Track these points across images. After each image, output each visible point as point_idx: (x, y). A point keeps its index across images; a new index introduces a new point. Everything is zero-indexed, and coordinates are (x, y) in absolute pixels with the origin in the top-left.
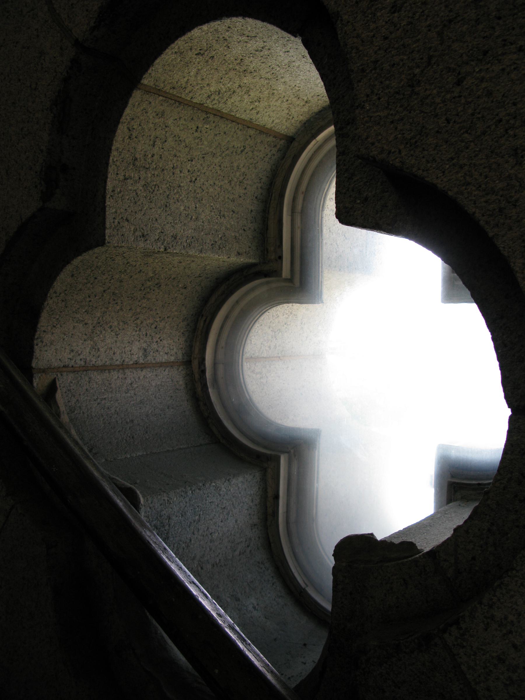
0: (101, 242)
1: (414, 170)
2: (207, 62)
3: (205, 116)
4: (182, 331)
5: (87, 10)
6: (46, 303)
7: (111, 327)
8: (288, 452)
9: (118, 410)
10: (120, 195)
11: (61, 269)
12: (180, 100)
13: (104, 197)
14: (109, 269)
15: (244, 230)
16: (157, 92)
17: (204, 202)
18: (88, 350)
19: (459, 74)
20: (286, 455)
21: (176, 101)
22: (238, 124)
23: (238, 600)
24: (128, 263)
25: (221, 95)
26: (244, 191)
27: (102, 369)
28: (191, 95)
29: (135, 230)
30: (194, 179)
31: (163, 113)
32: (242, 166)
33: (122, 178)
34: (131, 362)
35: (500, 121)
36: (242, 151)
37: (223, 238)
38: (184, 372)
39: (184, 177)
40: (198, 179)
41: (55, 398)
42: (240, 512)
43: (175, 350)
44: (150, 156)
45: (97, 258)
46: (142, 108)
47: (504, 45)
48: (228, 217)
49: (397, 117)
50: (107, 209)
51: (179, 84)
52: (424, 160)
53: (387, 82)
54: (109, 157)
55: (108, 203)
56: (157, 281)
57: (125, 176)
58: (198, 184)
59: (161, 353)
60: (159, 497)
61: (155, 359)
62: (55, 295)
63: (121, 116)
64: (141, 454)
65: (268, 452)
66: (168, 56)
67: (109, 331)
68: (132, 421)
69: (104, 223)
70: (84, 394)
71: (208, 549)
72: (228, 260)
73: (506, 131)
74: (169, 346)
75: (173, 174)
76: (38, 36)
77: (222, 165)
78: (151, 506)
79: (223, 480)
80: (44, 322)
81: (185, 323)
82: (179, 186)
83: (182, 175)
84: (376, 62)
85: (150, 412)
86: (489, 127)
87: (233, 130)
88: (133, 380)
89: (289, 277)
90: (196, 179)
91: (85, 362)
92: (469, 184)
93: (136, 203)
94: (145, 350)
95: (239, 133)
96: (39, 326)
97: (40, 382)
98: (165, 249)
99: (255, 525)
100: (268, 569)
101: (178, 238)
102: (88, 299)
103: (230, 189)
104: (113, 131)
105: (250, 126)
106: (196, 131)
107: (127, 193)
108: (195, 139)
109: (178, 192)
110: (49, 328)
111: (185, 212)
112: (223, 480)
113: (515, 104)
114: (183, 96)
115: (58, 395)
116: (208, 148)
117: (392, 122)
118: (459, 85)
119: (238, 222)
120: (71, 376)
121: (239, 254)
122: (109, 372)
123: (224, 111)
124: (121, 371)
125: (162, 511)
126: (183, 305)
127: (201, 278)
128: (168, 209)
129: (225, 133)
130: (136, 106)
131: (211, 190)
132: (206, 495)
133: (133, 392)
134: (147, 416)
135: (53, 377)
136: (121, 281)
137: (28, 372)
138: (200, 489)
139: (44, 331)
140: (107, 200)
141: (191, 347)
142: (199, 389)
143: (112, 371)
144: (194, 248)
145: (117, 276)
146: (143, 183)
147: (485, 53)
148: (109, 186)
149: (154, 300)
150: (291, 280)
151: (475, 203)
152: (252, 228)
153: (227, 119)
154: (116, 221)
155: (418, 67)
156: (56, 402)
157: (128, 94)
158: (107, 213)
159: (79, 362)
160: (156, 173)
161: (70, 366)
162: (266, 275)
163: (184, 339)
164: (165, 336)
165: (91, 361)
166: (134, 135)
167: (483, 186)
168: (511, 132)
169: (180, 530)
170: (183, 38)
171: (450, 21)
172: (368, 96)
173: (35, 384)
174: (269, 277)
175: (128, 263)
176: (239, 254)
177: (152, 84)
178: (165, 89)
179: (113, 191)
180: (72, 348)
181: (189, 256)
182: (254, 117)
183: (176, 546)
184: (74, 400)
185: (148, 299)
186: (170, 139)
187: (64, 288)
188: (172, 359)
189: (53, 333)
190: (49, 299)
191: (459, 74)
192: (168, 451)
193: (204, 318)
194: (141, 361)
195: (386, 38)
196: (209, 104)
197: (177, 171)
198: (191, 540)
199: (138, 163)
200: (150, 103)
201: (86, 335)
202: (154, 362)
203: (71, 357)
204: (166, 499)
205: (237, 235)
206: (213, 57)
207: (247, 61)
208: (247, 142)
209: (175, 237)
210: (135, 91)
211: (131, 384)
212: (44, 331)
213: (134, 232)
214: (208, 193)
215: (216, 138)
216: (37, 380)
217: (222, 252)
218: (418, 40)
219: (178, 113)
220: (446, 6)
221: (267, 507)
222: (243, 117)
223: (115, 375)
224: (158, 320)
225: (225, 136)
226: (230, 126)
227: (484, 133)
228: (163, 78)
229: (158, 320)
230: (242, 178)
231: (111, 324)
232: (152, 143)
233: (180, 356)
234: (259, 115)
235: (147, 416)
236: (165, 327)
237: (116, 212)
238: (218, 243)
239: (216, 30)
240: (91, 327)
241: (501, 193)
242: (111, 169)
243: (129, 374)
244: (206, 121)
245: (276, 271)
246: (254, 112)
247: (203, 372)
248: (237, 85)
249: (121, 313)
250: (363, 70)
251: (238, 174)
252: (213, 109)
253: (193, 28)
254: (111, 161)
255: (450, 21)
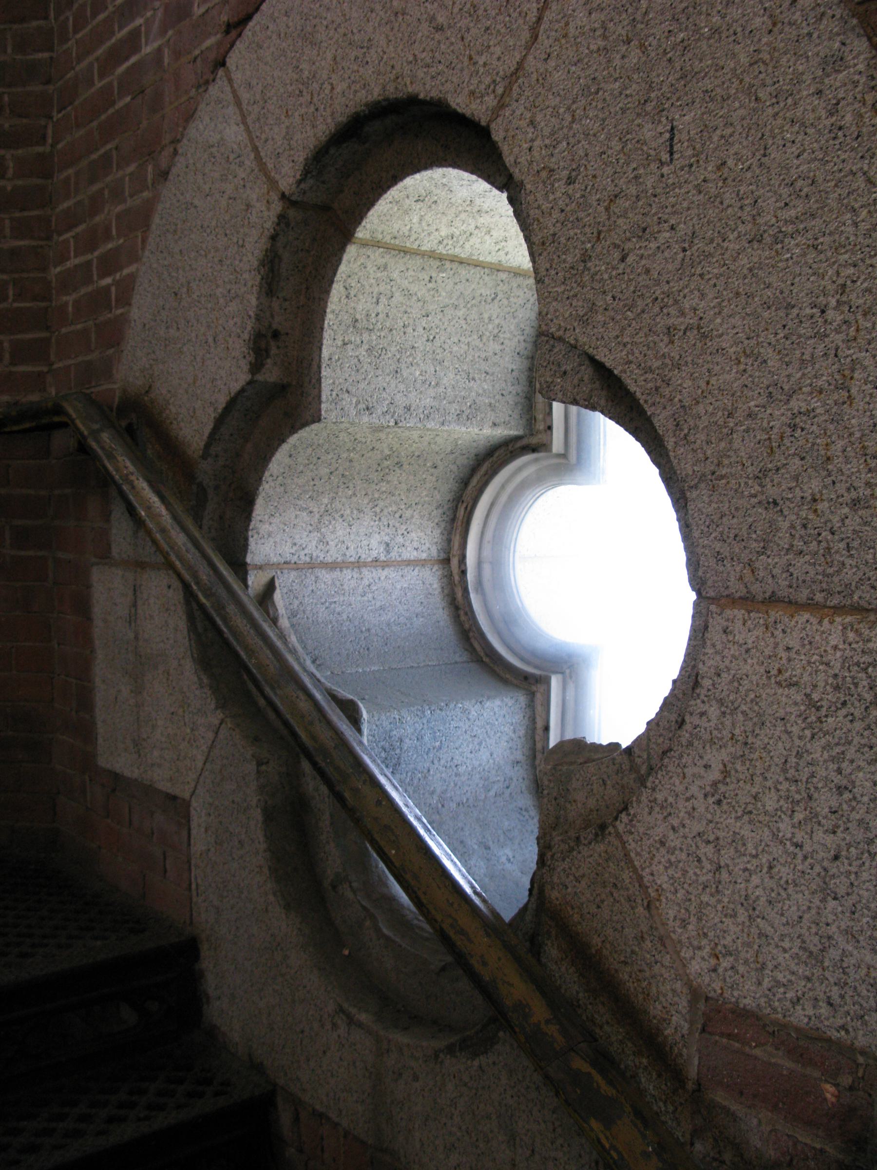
0: (317, 419)
1: (586, 347)
2: (430, 207)
3: (438, 263)
4: (436, 521)
5: (293, 161)
6: (261, 488)
7: (342, 516)
8: (562, 673)
9: (351, 616)
10: (339, 363)
11: (276, 449)
12: (406, 249)
13: (319, 367)
14: (334, 447)
15: (502, 395)
16: (377, 244)
17: (446, 363)
18: (314, 543)
19: (623, 250)
20: (560, 676)
21: (400, 251)
22: (484, 268)
23: (487, 848)
24: (355, 440)
25: (455, 239)
26: (501, 347)
27: (333, 566)
28: (417, 243)
29: (358, 403)
30: (431, 337)
31: (385, 267)
32: (495, 316)
33: (340, 343)
34: (370, 559)
35: (657, 299)
36: (493, 300)
37: (473, 407)
38: (439, 573)
39: (419, 336)
40: (437, 337)
41: (273, 599)
42: (496, 743)
43: (427, 545)
44: (373, 315)
45: (316, 435)
46: (359, 263)
47: (659, 223)
48: (480, 379)
49: (571, 294)
50: (323, 380)
51: (401, 233)
52: (594, 338)
53: (564, 257)
54: (323, 320)
55: (323, 373)
56: (396, 460)
57: (343, 340)
58: (437, 343)
59: (409, 549)
60: (388, 714)
61: (400, 556)
62: (271, 478)
63: (335, 274)
64: (376, 668)
65: (537, 672)
66: (383, 206)
67: (341, 520)
68: (369, 630)
69: (320, 396)
70: (309, 596)
71: (452, 784)
72: (481, 432)
73: (661, 308)
74: (421, 539)
75: (405, 333)
76: (244, 186)
77: (468, 318)
78: (378, 723)
79: (474, 701)
80: (260, 509)
81: (440, 511)
82: (413, 347)
83: (416, 334)
84: (554, 235)
85: (392, 620)
86: (647, 305)
87: (478, 276)
88: (372, 581)
89: (562, 452)
90: (434, 337)
91: (311, 558)
92: (631, 362)
93: (358, 371)
94: (388, 545)
95: (486, 278)
96: (254, 515)
97: (256, 581)
98: (396, 423)
99: (518, 762)
100: (533, 818)
101: (412, 409)
102: (312, 483)
103: (481, 346)
104: (328, 292)
105: (501, 268)
106: (430, 281)
107: (346, 360)
108: (429, 290)
109: (411, 355)
110: (266, 517)
111: (421, 377)
112: (474, 701)
113: (668, 282)
114: (408, 245)
115: (277, 596)
116: (447, 300)
117: (568, 298)
118: (623, 261)
119: (493, 386)
120: (293, 574)
121: (495, 424)
122: (341, 571)
123: (462, 255)
124: (355, 570)
125: (391, 731)
126: (435, 488)
127: (454, 455)
128: (398, 376)
129: (468, 280)
130: (352, 262)
131: (455, 349)
132: (450, 718)
133: (370, 595)
134: (388, 625)
135: (271, 576)
136: (351, 461)
137: (240, 568)
138: (441, 710)
139: (261, 521)
140: (323, 369)
141: (449, 541)
142: (459, 594)
143: (344, 569)
144: (433, 420)
145: (345, 455)
146: (367, 347)
147: (644, 230)
148: (325, 353)
149: (396, 482)
150: (564, 456)
151: (636, 382)
152: (514, 392)
153: (469, 264)
154: (334, 393)
155: (590, 242)
156: (273, 603)
157: (342, 249)
158: (323, 385)
159: (303, 557)
160: (383, 334)
161: (293, 562)
162: (534, 450)
163: (439, 531)
164: (413, 527)
165: (317, 557)
166: (352, 293)
167: (643, 365)
168: (665, 311)
169: (415, 756)
170: (395, 188)
171: (616, 196)
172: (547, 270)
173: (250, 583)
174: (538, 452)
175: (355, 440)
176: (495, 424)
177: (368, 236)
178: (384, 240)
179: (330, 359)
180: (295, 541)
181: (428, 430)
182: (503, 258)
183: (409, 774)
184: (296, 602)
185: (388, 482)
186: (397, 294)
187: (282, 470)
188: (424, 556)
189: (270, 524)
190: (264, 483)
191: (623, 250)
192: (412, 667)
193: (465, 505)
194: (383, 558)
195: (562, 211)
196: (441, 249)
197: (409, 330)
198: (429, 771)
199: (358, 325)
200: (369, 257)
201: (311, 525)
202: (399, 559)
203: (293, 551)
204: (397, 717)
205: (493, 401)
206: (436, 202)
207: (478, 201)
208: (499, 288)
209: (408, 408)
210: (349, 246)
211: (369, 586)
212: (261, 521)
213: (357, 405)
214: (451, 352)
215: (457, 287)
216: (253, 577)
217: (471, 423)
218: (589, 214)
219: (405, 264)
220: (612, 181)
221: (535, 741)
222: (489, 259)
223: (348, 573)
224: (403, 507)
225: (468, 284)
226: (472, 272)
227: (643, 311)
228: (380, 230)
229: (403, 507)
230: (496, 331)
231: (342, 512)
232: (375, 300)
233: (434, 552)
234: (509, 256)
235: (388, 625)
236: (412, 517)
237: (334, 383)
238: (466, 413)
239: (431, 178)
240: (317, 516)
241: (657, 372)
242: (327, 335)
243: (367, 573)
244: (441, 269)
245: (544, 445)
246: (501, 253)
247: (464, 573)
248: (473, 226)
249: (354, 499)
250: (543, 244)
251: (490, 327)
252: (448, 255)
253: (404, 178)
254: (326, 325)
255: (616, 196)
